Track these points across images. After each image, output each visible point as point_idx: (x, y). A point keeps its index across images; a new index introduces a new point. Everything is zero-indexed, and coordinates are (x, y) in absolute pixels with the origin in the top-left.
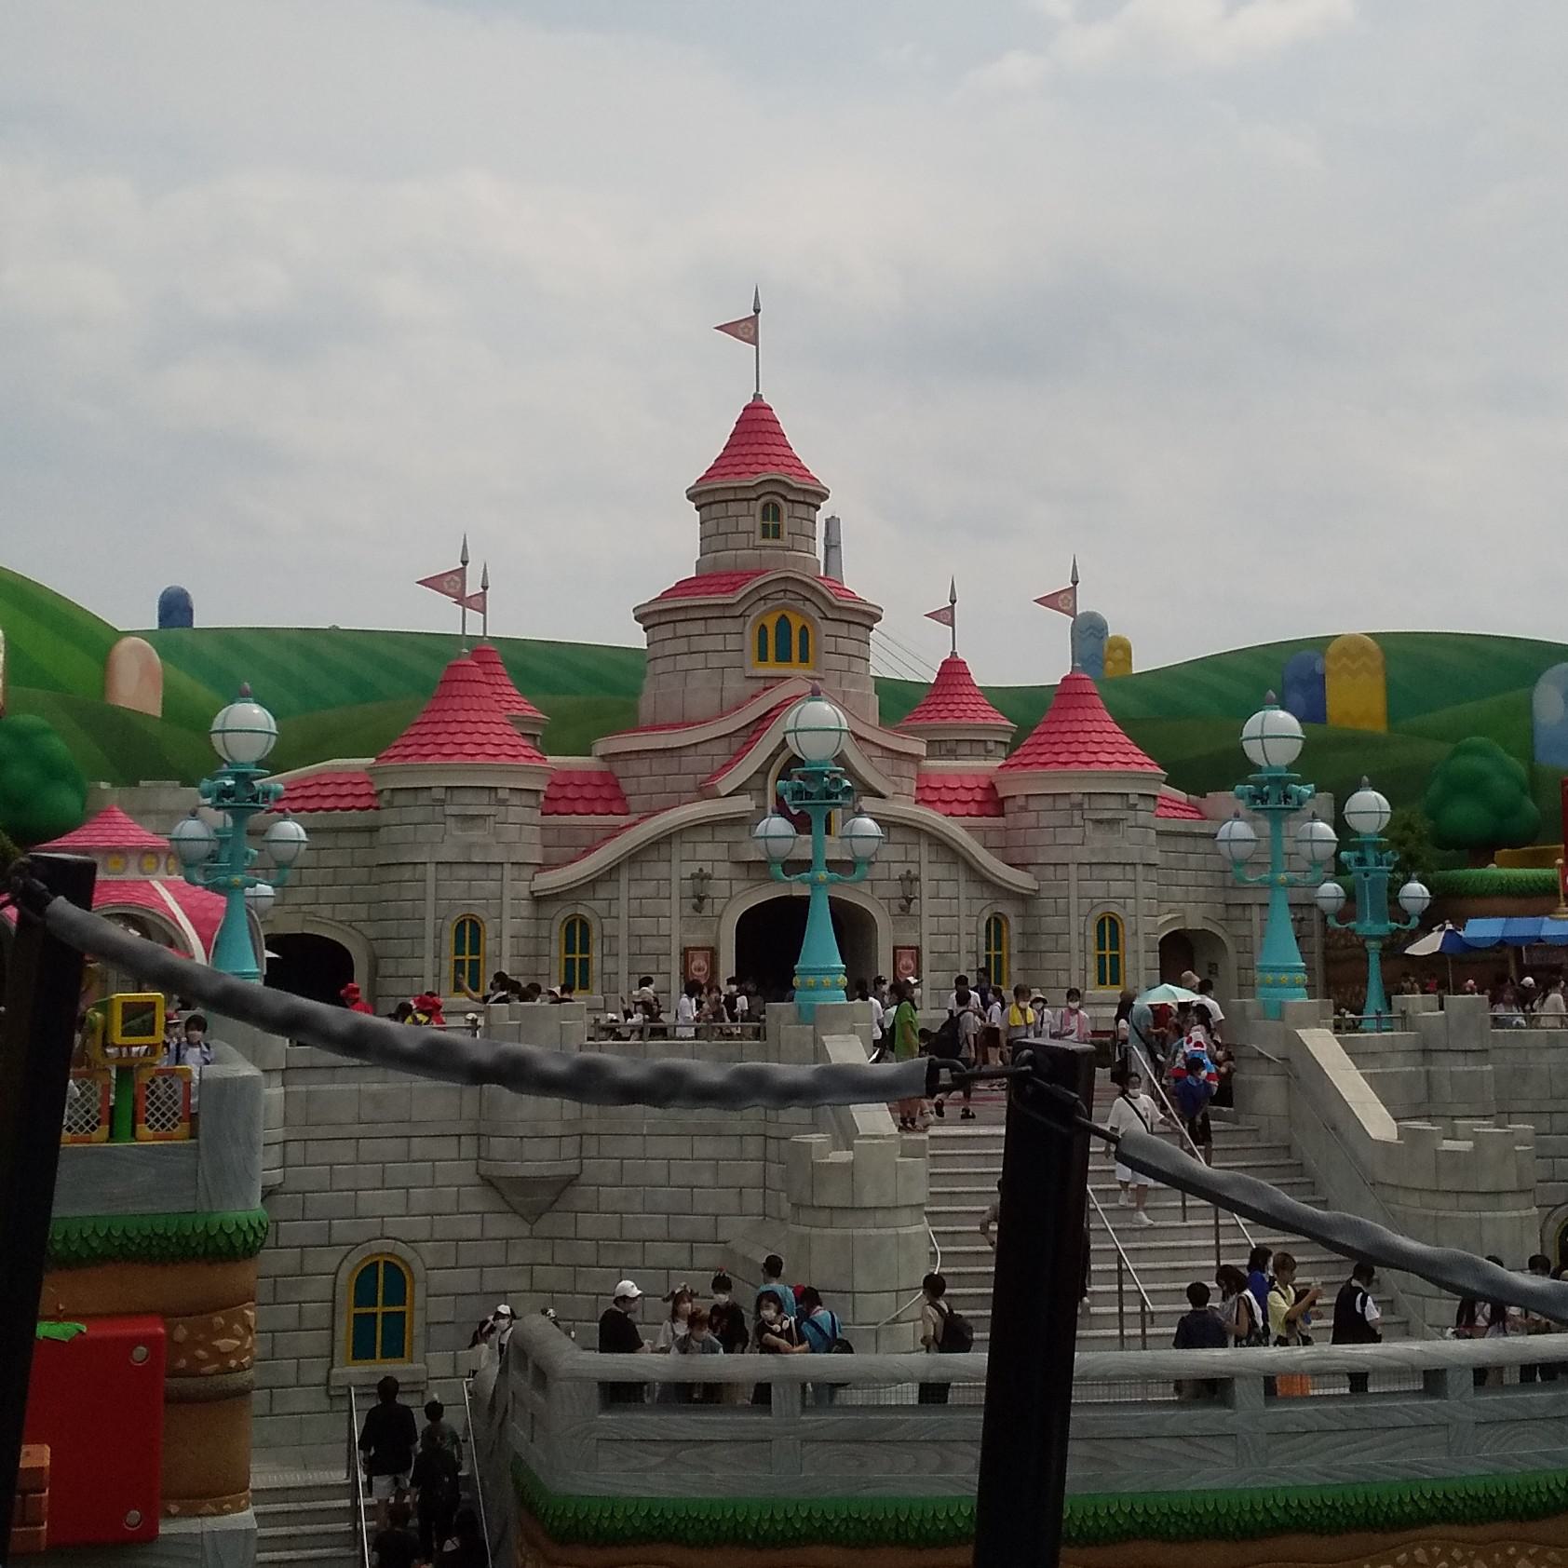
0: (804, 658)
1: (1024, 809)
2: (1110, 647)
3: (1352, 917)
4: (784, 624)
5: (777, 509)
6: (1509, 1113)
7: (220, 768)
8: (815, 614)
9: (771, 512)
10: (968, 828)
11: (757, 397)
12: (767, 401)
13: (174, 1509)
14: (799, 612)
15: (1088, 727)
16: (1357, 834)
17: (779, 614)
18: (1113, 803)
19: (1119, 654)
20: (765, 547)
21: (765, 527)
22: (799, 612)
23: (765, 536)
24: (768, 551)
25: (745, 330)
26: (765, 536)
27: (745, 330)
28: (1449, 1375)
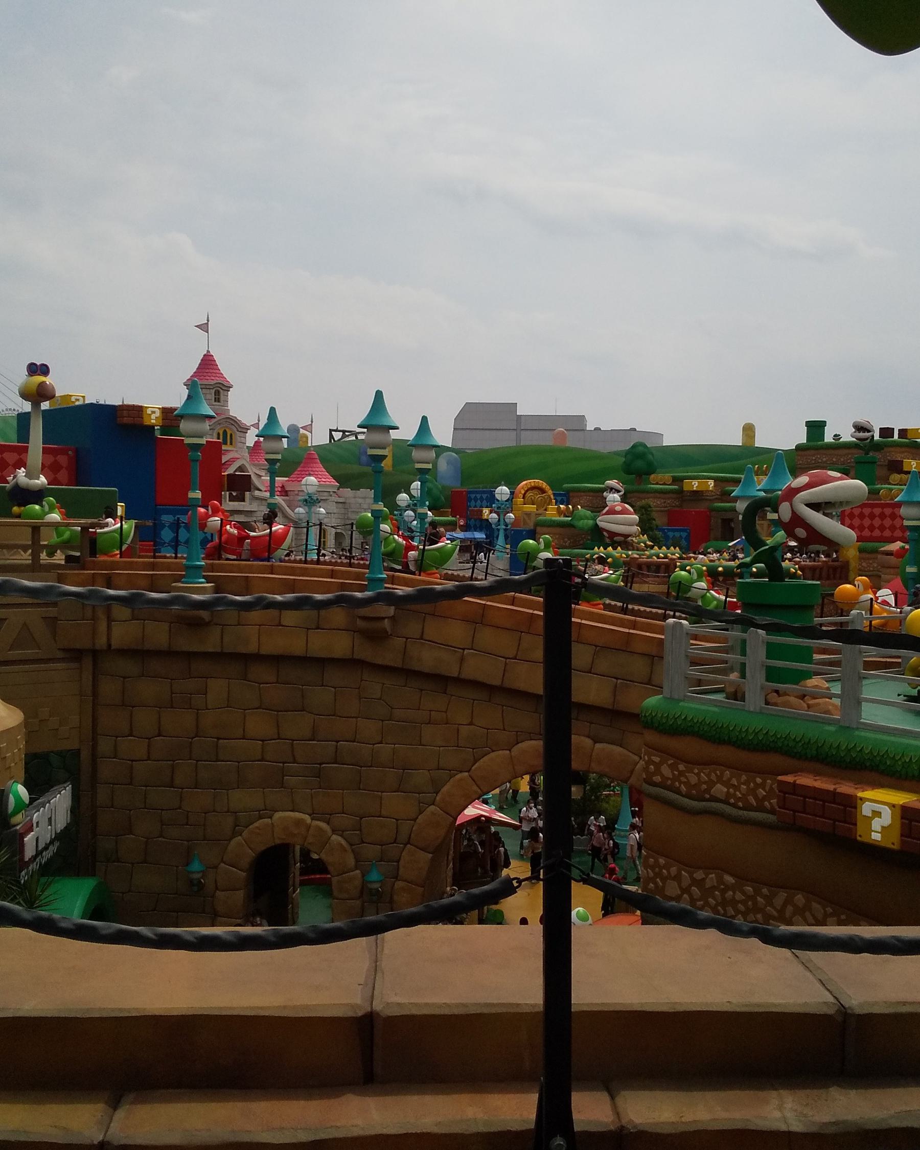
0: (231, 444)
1: (298, 495)
2: (302, 437)
3: (499, 525)
4: (225, 432)
5: (219, 392)
6: (172, 693)
7: (38, 478)
8: (235, 429)
9: (217, 393)
10: (283, 500)
11: (208, 351)
12: (212, 353)
13: (561, 561)
14: (230, 429)
15: (317, 469)
16: (399, 506)
17: (223, 429)
18: (326, 494)
19: (304, 439)
20: (216, 405)
21: (215, 398)
22: (230, 429)
23: (215, 401)
24: (217, 407)
25: (204, 327)
26: (215, 401)
27: (204, 327)
28: (909, 431)
